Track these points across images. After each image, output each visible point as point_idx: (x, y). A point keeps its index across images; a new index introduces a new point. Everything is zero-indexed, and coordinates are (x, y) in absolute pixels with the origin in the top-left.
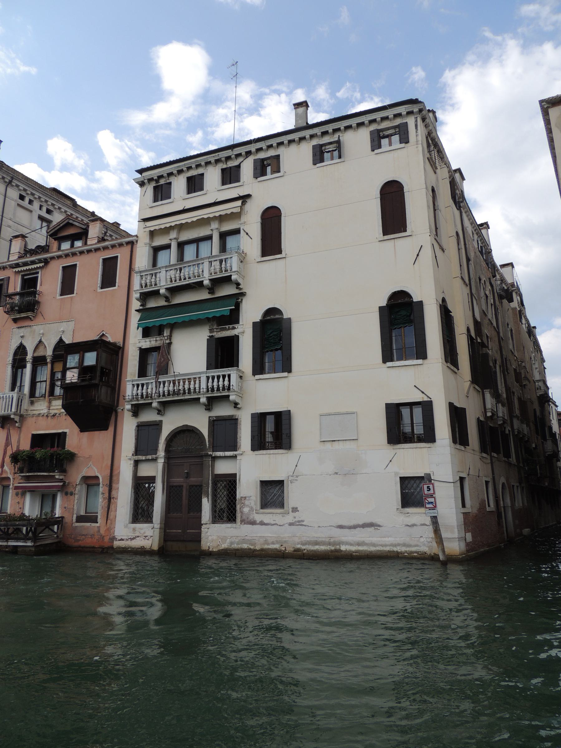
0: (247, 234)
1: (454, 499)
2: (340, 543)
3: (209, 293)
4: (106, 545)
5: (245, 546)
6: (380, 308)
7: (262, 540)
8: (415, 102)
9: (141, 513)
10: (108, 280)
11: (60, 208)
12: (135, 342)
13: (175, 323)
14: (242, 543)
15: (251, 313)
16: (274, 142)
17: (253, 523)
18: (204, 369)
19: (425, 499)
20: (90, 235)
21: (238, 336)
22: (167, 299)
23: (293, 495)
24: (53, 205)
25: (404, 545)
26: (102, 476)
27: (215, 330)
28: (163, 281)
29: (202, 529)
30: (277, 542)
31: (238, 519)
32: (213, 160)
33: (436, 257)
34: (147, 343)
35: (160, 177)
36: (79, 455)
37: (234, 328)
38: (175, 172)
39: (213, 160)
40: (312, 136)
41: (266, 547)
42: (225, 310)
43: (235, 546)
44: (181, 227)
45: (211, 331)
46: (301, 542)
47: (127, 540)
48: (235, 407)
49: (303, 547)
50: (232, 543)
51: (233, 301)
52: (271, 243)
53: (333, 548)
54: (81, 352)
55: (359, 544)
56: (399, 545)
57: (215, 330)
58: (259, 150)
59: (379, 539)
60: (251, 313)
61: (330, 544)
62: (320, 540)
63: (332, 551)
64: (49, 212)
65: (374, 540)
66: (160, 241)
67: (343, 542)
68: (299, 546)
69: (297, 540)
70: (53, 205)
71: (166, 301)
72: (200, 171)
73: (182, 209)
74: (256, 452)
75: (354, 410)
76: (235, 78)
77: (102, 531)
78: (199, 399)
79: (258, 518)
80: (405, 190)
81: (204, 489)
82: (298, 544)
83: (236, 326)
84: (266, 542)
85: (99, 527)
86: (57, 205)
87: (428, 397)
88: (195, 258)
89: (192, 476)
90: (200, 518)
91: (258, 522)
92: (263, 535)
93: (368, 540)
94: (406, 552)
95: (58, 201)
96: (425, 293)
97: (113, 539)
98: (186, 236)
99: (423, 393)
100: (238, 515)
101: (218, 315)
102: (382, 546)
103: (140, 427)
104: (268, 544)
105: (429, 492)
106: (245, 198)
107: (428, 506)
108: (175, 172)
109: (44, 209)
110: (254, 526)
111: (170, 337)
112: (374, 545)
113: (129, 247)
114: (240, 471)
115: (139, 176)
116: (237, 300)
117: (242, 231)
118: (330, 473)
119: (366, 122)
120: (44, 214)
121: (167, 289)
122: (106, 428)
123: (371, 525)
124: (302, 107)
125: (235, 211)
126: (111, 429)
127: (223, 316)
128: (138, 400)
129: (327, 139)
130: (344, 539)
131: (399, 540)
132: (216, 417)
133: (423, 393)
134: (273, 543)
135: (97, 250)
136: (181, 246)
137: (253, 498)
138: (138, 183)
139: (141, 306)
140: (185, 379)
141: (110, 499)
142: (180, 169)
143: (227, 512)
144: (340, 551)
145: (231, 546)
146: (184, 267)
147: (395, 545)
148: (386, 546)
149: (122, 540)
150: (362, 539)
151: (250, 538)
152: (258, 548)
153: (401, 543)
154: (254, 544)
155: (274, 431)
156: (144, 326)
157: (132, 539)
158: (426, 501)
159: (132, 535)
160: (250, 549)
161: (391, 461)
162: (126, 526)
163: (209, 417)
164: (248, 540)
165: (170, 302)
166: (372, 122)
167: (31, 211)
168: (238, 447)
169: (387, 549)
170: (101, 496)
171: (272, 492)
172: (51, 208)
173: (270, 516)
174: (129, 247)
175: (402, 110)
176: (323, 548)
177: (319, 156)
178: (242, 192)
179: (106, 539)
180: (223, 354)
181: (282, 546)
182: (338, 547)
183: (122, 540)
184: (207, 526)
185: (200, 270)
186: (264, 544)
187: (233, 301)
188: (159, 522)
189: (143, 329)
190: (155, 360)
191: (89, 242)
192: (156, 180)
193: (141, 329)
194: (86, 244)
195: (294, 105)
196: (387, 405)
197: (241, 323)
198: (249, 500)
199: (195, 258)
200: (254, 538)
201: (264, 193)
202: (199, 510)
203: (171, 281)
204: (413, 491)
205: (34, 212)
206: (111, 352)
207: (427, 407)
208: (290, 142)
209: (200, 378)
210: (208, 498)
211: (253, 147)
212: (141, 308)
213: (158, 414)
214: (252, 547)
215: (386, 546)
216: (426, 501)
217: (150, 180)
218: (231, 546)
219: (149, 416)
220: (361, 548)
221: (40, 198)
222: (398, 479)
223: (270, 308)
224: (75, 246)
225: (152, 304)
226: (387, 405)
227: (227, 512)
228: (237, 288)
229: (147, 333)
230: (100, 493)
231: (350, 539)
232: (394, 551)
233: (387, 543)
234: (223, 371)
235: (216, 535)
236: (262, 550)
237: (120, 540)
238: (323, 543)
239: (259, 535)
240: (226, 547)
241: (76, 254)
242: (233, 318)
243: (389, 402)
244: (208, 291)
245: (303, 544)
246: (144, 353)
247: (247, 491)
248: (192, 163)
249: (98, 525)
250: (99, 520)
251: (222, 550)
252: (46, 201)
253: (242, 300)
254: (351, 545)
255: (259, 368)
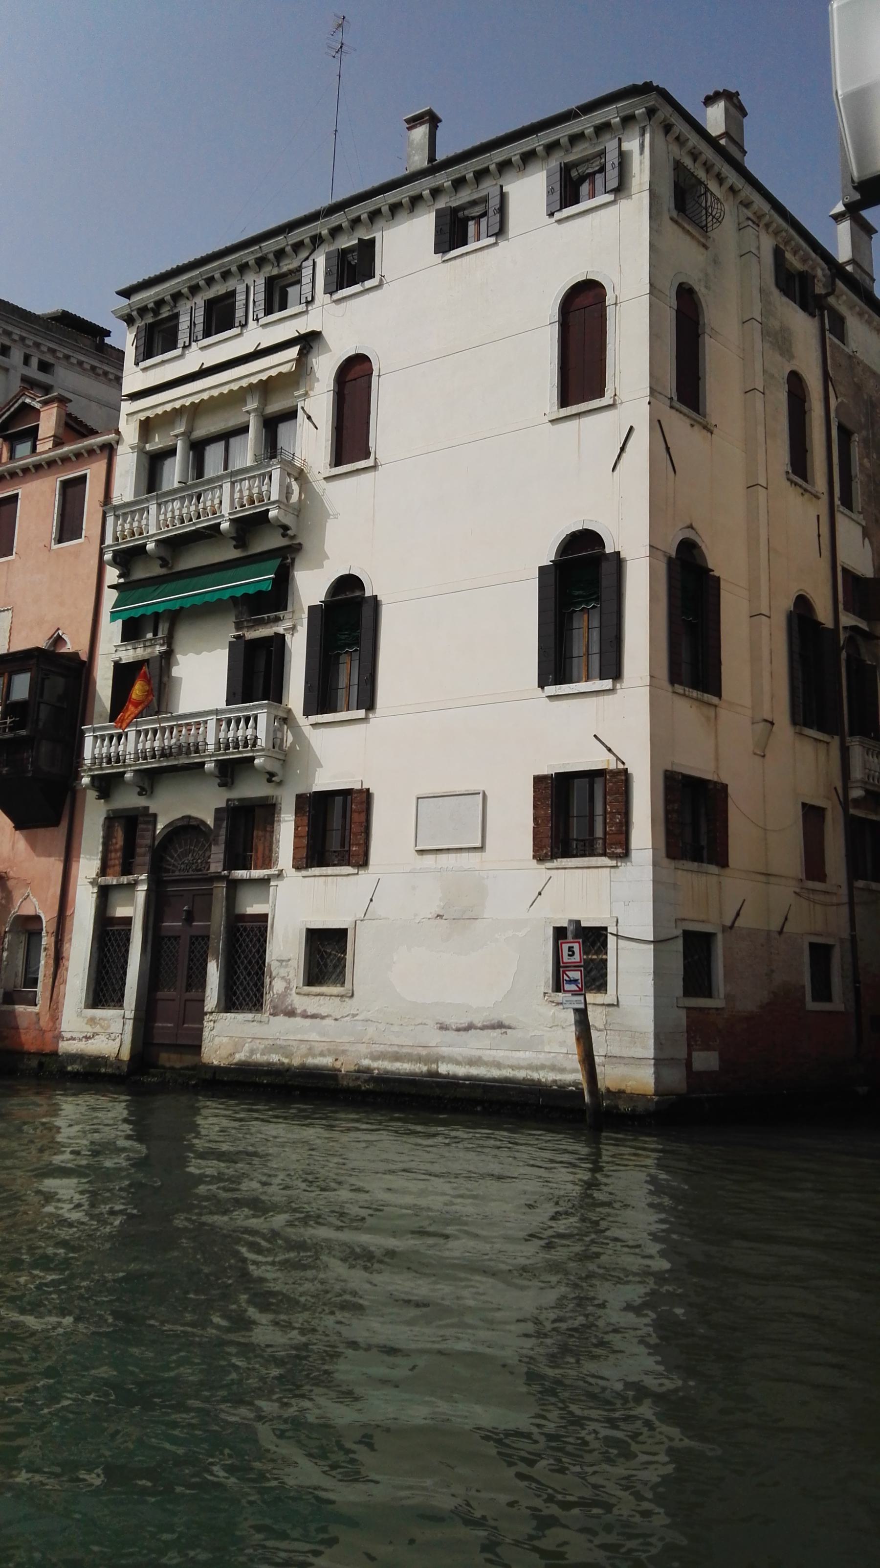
0: (309, 418)
1: (652, 977)
2: (438, 1059)
3: (236, 547)
4: (47, 1049)
5: (275, 1058)
6: (541, 569)
7: (304, 1048)
8: (647, 88)
9: (104, 990)
10: (69, 527)
11: (67, 357)
12: (111, 649)
13: (182, 608)
14: (270, 1053)
15: (311, 587)
16: (362, 210)
17: (291, 1013)
18: (222, 705)
19: (564, 972)
20: (41, 435)
21: (284, 635)
22: (164, 563)
23: (362, 956)
24: (53, 351)
25: (553, 1068)
26: (48, 917)
27: (245, 624)
28: (154, 524)
29: (205, 1023)
30: (330, 1052)
31: (267, 1006)
32: (251, 259)
33: (668, 449)
34: (128, 655)
35: (160, 303)
36: (11, 874)
37: (277, 620)
38: (185, 291)
39: (251, 259)
40: (436, 192)
41: (311, 1061)
42: (262, 579)
43: (259, 1058)
44: (195, 411)
45: (239, 626)
46: (371, 1053)
47: (80, 1040)
48: (269, 781)
49: (375, 1065)
50: (252, 1052)
51: (275, 563)
52: (351, 440)
53: (425, 1069)
54: (6, 675)
55: (471, 1062)
56: (543, 1067)
57: (245, 624)
58: (336, 231)
59: (508, 1053)
60: (311, 587)
61: (419, 1059)
62: (404, 1050)
63: (422, 1075)
64: (44, 367)
65: (499, 1055)
66: (157, 443)
67: (444, 1057)
68: (366, 1062)
69: (363, 1049)
70: (53, 351)
71: (162, 566)
72: (232, 284)
73: (196, 368)
74: (304, 873)
75: (480, 788)
76: (338, 55)
77: (44, 1022)
78: (203, 764)
79: (300, 1003)
80: (609, 299)
81: (212, 943)
82: (366, 1057)
83: (281, 614)
84: (311, 1052)
85: (38, 1014)
86: (63, 351)
87: (618, 759)
88: (222, 472)
89: (192, 920)
90: (202, 1001)
91: (299, 1011)
92: (306, 1038)
93: (488, 1055)
94: (555, 1081)
95: (60, 343)
96: (630, 536)
97: (59, 1037)
98: (206, 428)
99: (610, 750)
100: (267, 998)
101: (251, 591)
102: (513, 1067)
103: (110, 821)
104: (314, 1056)
105: (572, 960)
106: (308, 342)
107: (567, 987)
108: (185, 291)
109: (34, 362)
110: (292, 1019)
111: (169, 640)
112: (499, 1065)
113: (106, 453)
114: (274, 910)
115: (125, 302)
116: (285, 560)
117: (300, 412)
118: (430, 916)
119: (516, 159)
120: (33, 372)
121: (159, 542)
122: (56, 823)
123: (500, 1026)
124: (421, 124)
125: (285, 369)
126: (64, 824)
127: (260, 592)
128: (102, 769)
129: (465, 196)
130: (445, 1051)
131: (541, 1058)
132: (239, 800)
133: (610, 750)
134: (322, 1054)
135: (51, 463)
136: (198, 448)
137: (293, 963)
138: (122, 318)
139: (119, 577)
140: (180, 726)
141: (59, 958)
142: (193, 283)
143: (246, 989)
144: (437, 1074)
145: (251, 1057)
146: (205, 491)
147: (537, 1068)
148: (520, 1068)
149: (73, 1039)
150: (477, 1053)
151: (285, 1043)
152: (296, 1062)
153: (548, 1063)
154: (289, 1055)
155: (337, 829)
156: (126, 615)
157: (87, 1038)
158: (566, 977)
159: (89, 1030)
160: (283, 1064)
161: (540, 894)
162: (80, 1015)
163: (228, 800)
164: (281, 1047)
165: (171, 568)
166: (552, 147)
167: (7, 370)
168: (273, 859)
169: (521, 1074)
170: (43, 954)
171: (327, 953)
172: (49, 358)
173: (323, 1000)
174: (106, 453)
175: (611, 114)
176: (405, 1067)
177: (452, 234)
178: (302, 326)
179: (48, 1036)
180: (255, 674)
181: (336, 1060)
182: (434, 1066)
183: (73, 1039)
184: (214, 1017)
185: (217, 501)
186: (306, 1056)
187: (275, 563)
188: (133, 1007)
189: (124, 622)
190: (146, 686)
191: (40, 448)
192: (152, 309)
193: (119, 623)
194: (34, 449)
195: (408, 121)
196: (539, 781)
197: (290, 609)
198: (286, 966)
199: (222, 472)
200: (290, 1043)
201: (344, 323)
202: (202, 984)
203: (182, 522)
204: (582, 955)
205: (12, 371)
206: (79, 670)
207: (618, 781)
208: (395, 208)
209: (206, 722)
210: (217, 962)
211: (322, 227)
212: (122, 580)
213: (140, 794)
214: (286, 1061)
215: (520, 1068)
216: (566, 977)
217: (143, 311)
218: (251, 1057)
219: (128, 800)
220: (474, 1071)
221: (23, 339)
222: (550, 932)
223: (342, 577)
224: (17, 456)
225: (139, 574)
226: (539, 781)
227: (246, 989)
228: (284, 535)
229: (132, 631)
230: (43, 947)
231: (455, 1051)
232: (533, 1080)
233: (522, 1063)
234: (246, 709)
235: (229, 1038)
236: (303, 1067)
237: (69, 1039)
238: (408, 1058)
239: (299, 1037)
240: (243, 1058)
241: (17, 474)
242: (278, 597)
243: (536, 774)
244: (234, 543)
245: (375, 1058)
246: (124, 674)
247: (285, 950)
248: (213, 270)
249: (36, 1009)
250: (39, 1000)
251: (236, 1064)
252: (37, 345)
253: (293, 560)
254: (458, 1063)
255: (321, 700)
